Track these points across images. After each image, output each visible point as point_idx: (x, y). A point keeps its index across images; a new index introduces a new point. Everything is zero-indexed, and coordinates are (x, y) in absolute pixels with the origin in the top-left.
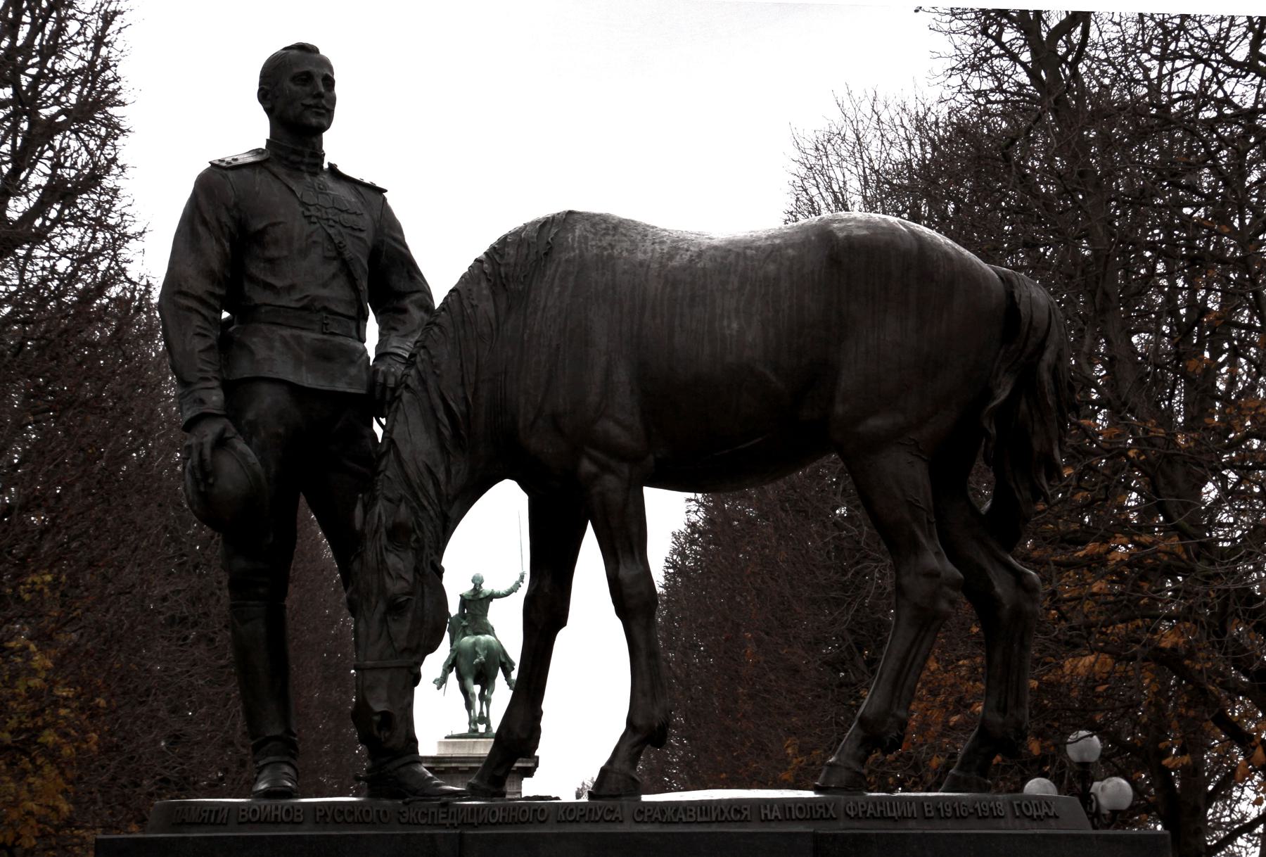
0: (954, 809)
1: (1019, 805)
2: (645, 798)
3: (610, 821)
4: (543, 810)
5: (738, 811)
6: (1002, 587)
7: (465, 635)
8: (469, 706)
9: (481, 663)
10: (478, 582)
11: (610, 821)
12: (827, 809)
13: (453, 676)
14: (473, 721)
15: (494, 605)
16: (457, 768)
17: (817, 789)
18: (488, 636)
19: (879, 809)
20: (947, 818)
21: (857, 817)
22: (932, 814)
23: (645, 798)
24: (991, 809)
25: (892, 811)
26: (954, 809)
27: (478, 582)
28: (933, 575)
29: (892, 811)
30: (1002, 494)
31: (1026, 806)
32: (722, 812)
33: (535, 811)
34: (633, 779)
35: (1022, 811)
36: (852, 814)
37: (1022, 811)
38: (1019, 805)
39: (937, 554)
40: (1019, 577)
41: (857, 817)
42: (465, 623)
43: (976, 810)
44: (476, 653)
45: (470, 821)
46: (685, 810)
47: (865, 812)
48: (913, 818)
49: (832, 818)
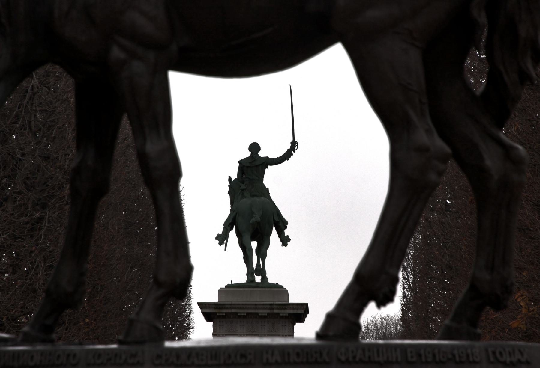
0: (434, 356)
1: (494, 353)
2: (168, 344)
3: (133, 364)
4: (75, 355)
5: (243, 356)
6: (492, 161)
7: (243, 197)
8: (247, 259)
9: (258, 223)
10: (255, 148)
11: (133, 364)
12: (321, 354)
13: (233, 234)
14: (251, 273)
15: (270, 173)
16: (236, 313)
17: (120, 342)
18: (263, 198)
19: (367, 354)
20: (427, 362)
21: (347, 361)
22: (415, 359)
23: (168, 344)
24: (468, 356)
25: (378, 356)
26: (434, 356)
27: (255, 148)
28: (423, 150)
29: (378, 356)
30: (494, 77)
31: (501, 353)
32: (230, 356)
33: (68, 355)
34: (157, 329)
35: (496, 358)
36: (343, 358)
37: (496, 358)
38: (494, 353)
39: (428, 131)
40: (507, 150)
41: (347, 361)
42: (243, 187)
43: (454, 356)
44: (253, 213)
45: (376, 359)
46: (189, 356)
47: (354, 357)
48: (397, 362)
49: (325, 362)
